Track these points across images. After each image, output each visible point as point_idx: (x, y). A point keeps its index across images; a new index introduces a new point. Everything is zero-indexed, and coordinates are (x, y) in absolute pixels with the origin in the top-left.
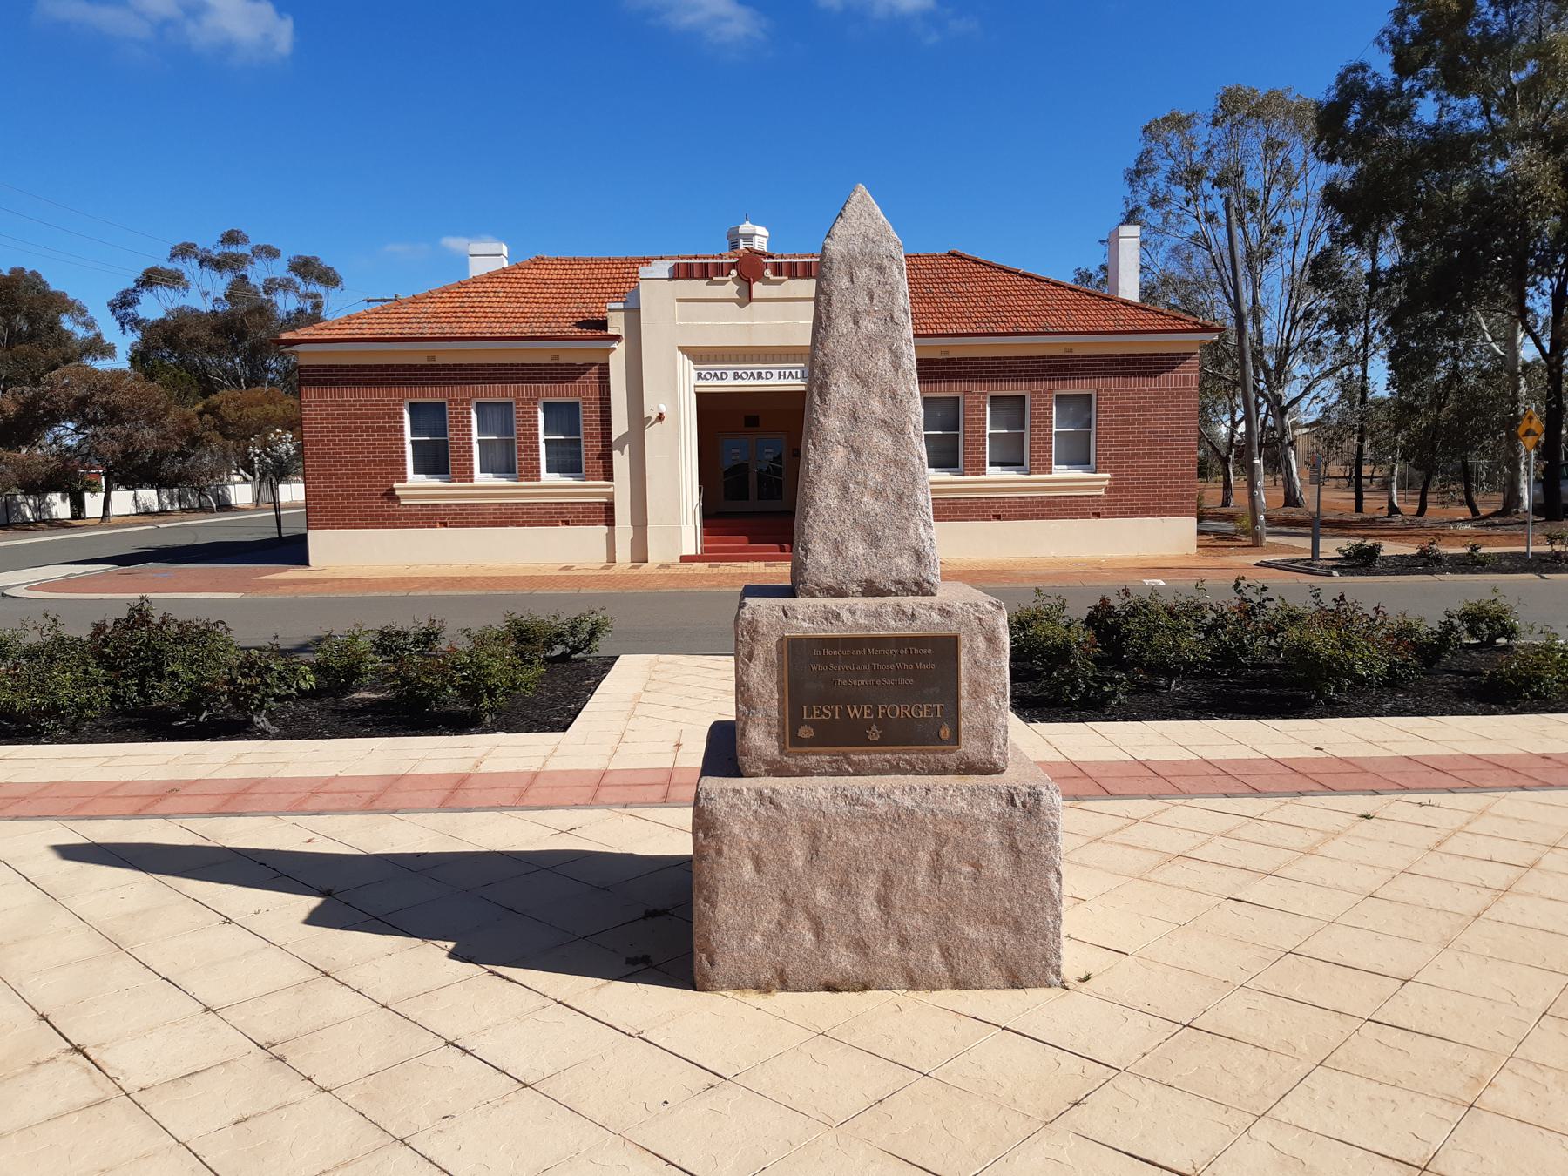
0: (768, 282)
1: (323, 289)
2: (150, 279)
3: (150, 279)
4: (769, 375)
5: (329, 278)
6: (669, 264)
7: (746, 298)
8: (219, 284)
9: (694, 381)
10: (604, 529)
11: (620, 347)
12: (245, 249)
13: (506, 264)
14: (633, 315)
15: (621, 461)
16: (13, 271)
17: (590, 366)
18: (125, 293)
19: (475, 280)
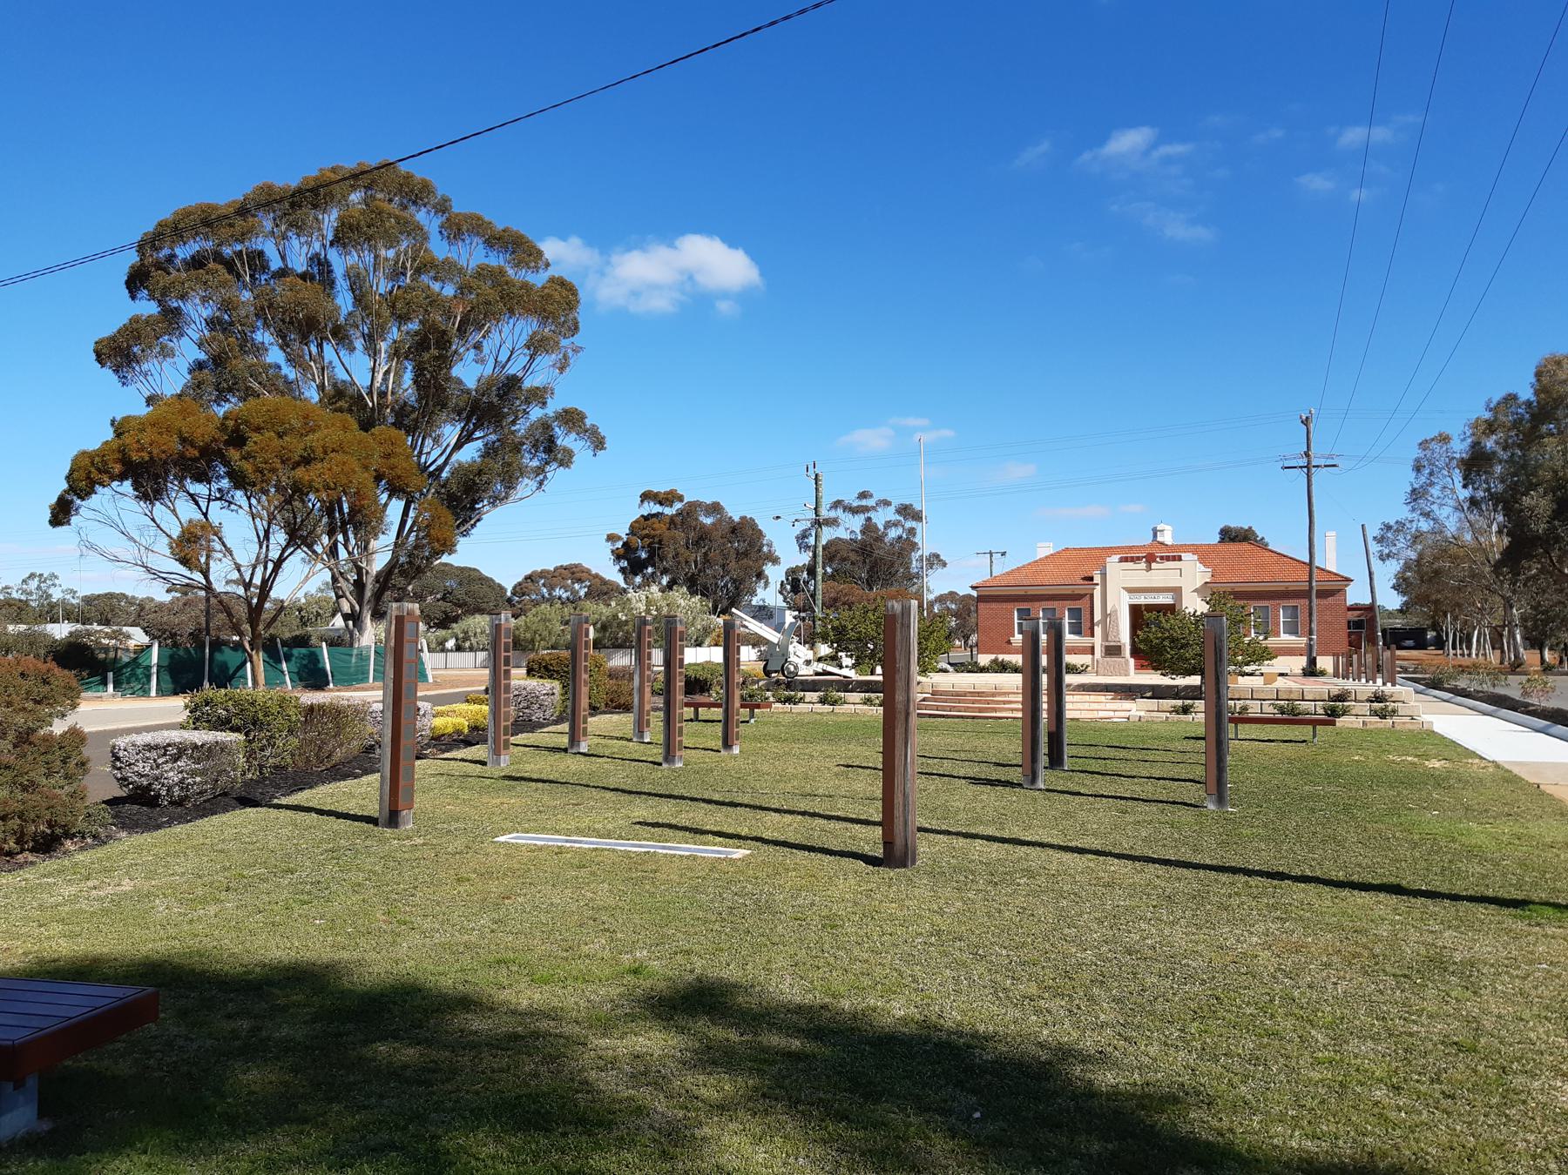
4: (1158, 598)
5: (917, 517)
6: (1119, 556)
7: (1149, 569)
10: (1091, 656)
11: (1098, 588)
12: (870, 502)
14: (1104, 575)
15: (1098, 630)
16: (743, 518)
17: (1084, 595)
19: (1041, 559)
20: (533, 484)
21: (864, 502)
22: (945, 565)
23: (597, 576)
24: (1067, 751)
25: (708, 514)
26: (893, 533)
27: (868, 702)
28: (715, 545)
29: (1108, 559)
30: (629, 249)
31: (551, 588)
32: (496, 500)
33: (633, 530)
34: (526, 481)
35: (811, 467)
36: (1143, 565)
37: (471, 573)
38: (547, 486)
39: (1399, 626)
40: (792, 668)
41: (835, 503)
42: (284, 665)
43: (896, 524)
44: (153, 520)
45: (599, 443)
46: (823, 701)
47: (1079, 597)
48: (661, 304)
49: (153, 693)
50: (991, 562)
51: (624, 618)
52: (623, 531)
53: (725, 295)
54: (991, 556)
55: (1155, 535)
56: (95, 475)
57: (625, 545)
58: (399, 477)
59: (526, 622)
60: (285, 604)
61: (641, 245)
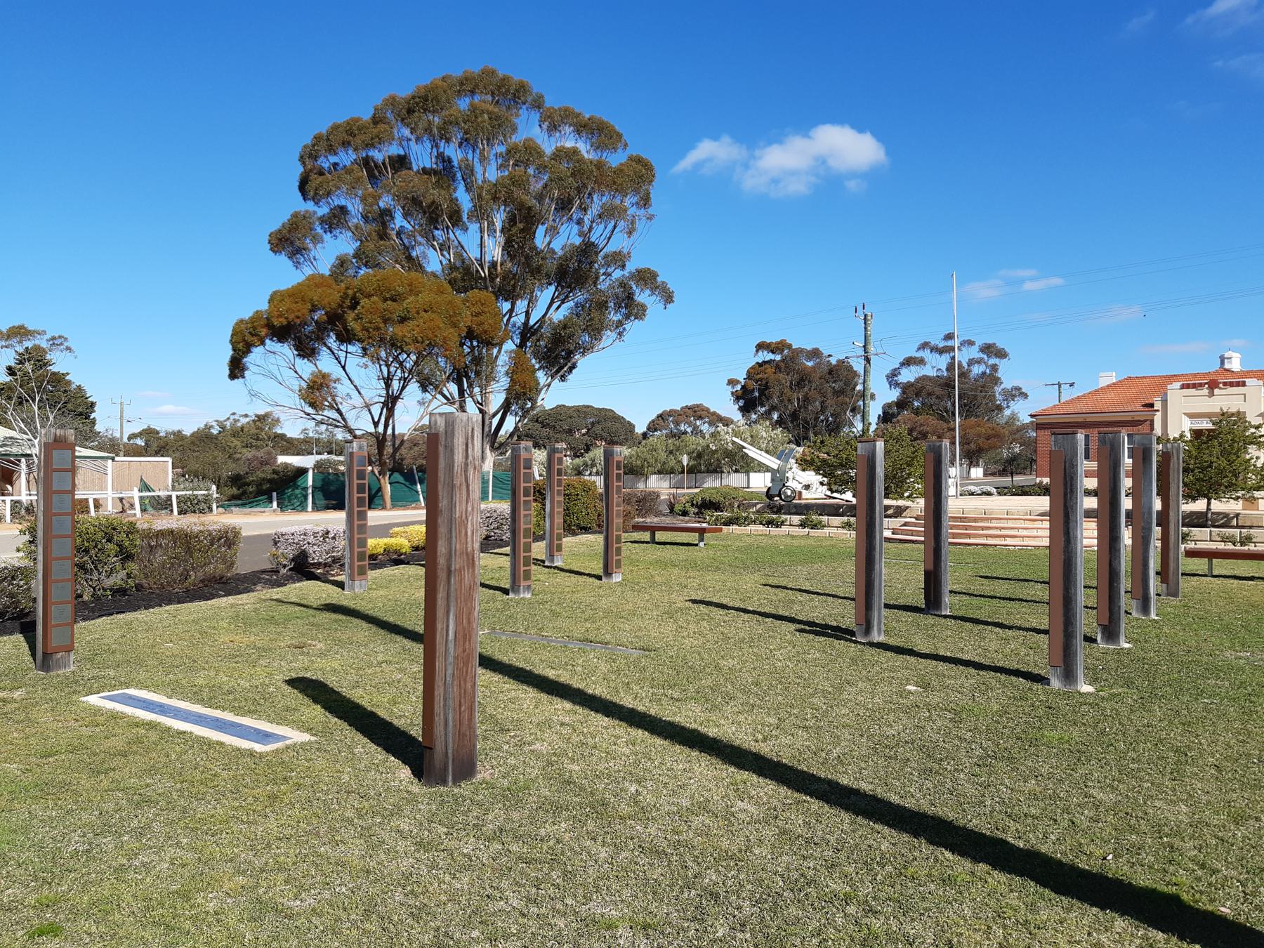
0: (1221, 388)
1: (998, 360)
2: (908, 362)
3: (908, 362)
5: (1002, 354)
7: (1212, 394)
8: (942, 362)
9: (1189, 425)
11: (1159, 414)
13: (1114, 381)
14: (1165, 402)
18: (895, 370)
19: (1102, 388)
20: (614, 335)
21: (949, 343)
22: (1026, 396)
23: (714, 413)
24: (947, 599)
25: (809, 359)
26: (977, 370)
27: (847, 525)
28: (814, 386)
29: (1169, 387)
30: (770, 142)
31: (677, 424)
32: (586, 350)
33: (750, 375)
34: (608, 333)
35: (860, 308)
36: (1205, 391)
37: (607, 413)
38: (626, 337)
39: (456, 458)
40: (789, 493)
41: (923, 344)
42: (419, 486)
43: (979, 362)
44: (296, 372)
45: (668, 298)
46: (803, 525)
47: (1140, 423)
48: (797, 187)
49: (310, 508)
50: (1060, 392)
51: (714, 448)
52: (741, 376)
53: (853, 175)
54: (1060, 386)
55: (1222, 363)
56: (249, 338)
57: (743, 387)
58: (486, 332)
59: (637, 452)
60: (405, 438)
61: (778, 140)
